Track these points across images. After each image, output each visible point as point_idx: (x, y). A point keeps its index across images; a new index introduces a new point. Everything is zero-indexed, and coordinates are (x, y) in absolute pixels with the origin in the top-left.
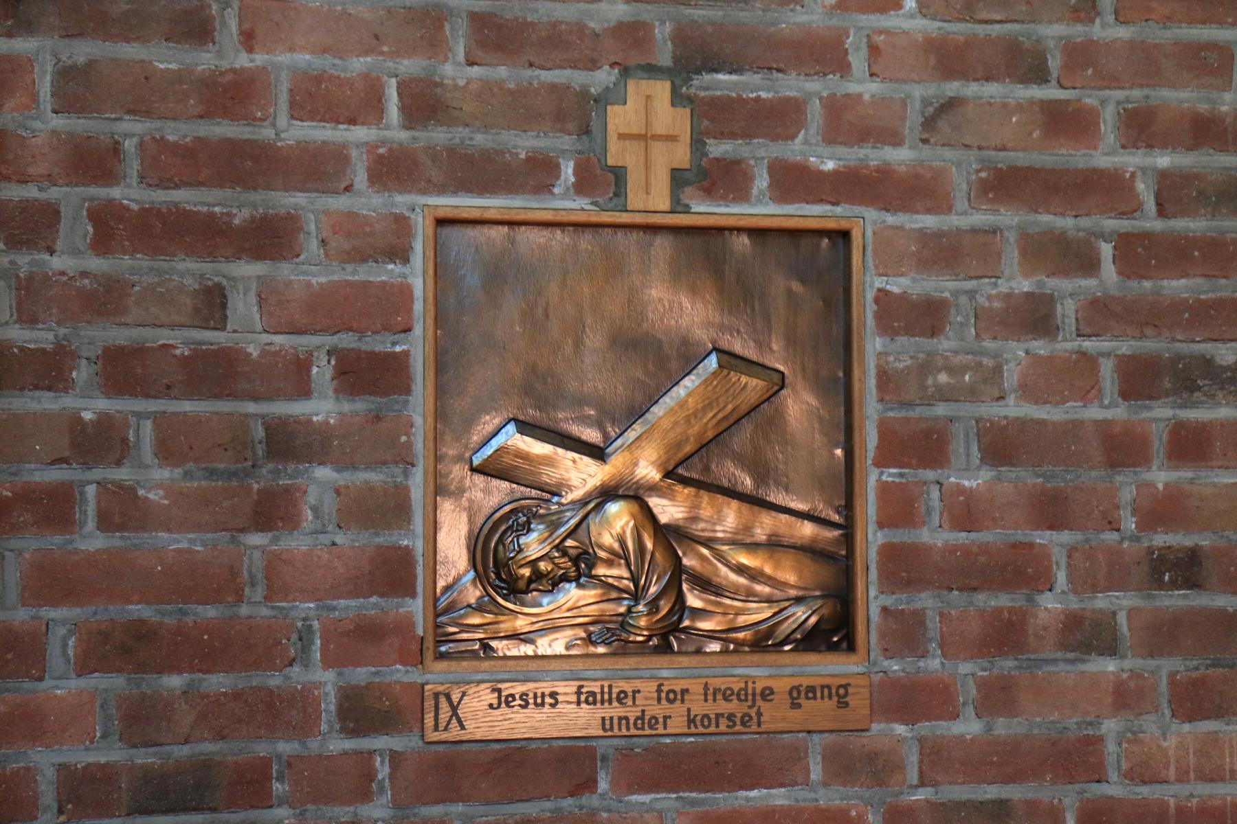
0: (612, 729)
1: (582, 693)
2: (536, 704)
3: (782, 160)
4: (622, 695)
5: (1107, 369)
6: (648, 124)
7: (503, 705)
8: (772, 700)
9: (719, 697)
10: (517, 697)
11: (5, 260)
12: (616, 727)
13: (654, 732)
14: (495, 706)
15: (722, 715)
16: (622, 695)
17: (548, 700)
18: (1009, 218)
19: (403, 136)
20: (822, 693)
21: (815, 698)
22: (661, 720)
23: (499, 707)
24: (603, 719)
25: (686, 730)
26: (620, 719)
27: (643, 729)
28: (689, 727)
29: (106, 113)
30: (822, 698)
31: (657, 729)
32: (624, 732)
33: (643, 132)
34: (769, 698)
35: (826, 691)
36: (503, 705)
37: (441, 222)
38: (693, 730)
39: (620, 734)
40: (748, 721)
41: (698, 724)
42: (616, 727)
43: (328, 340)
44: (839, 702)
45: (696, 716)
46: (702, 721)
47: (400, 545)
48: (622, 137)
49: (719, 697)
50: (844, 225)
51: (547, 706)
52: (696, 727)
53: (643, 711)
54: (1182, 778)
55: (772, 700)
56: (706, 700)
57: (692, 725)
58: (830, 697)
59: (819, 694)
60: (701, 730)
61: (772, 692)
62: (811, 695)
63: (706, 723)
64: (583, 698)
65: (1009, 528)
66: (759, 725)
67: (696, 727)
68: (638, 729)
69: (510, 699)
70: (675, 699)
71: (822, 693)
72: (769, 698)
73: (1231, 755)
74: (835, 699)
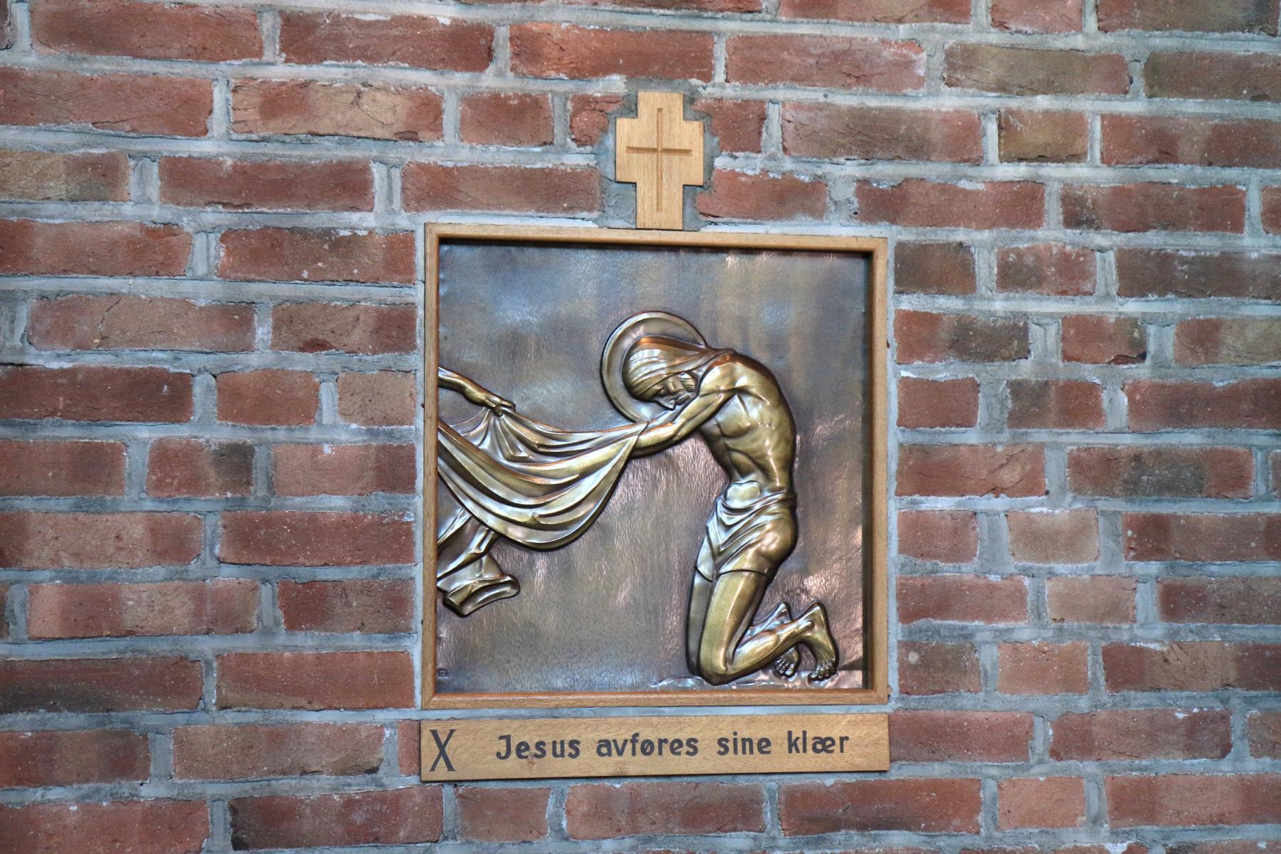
2: (555, 754)
4: (764, 744)
6: (659, 139)
7: (513, 755)
8: (769, 752)
9: (666, 748)
10: (684, 742)
11: (1171, 1)
16: (764, 744)
17: (568, 750)
20: (563, 750)
21: (609, 754)
23: (505, 757)
33: (655, 147)
34: (830, 749)
35: (558, 751)
36: (513, 755)
37: (444, 240)
48: (631, 149)
49: (666, 748)
50: (865, 245)
61: (768, 743)
65: (1189, 560)
69: (523, 748)
72: (830, 749)
73: (212, 815)
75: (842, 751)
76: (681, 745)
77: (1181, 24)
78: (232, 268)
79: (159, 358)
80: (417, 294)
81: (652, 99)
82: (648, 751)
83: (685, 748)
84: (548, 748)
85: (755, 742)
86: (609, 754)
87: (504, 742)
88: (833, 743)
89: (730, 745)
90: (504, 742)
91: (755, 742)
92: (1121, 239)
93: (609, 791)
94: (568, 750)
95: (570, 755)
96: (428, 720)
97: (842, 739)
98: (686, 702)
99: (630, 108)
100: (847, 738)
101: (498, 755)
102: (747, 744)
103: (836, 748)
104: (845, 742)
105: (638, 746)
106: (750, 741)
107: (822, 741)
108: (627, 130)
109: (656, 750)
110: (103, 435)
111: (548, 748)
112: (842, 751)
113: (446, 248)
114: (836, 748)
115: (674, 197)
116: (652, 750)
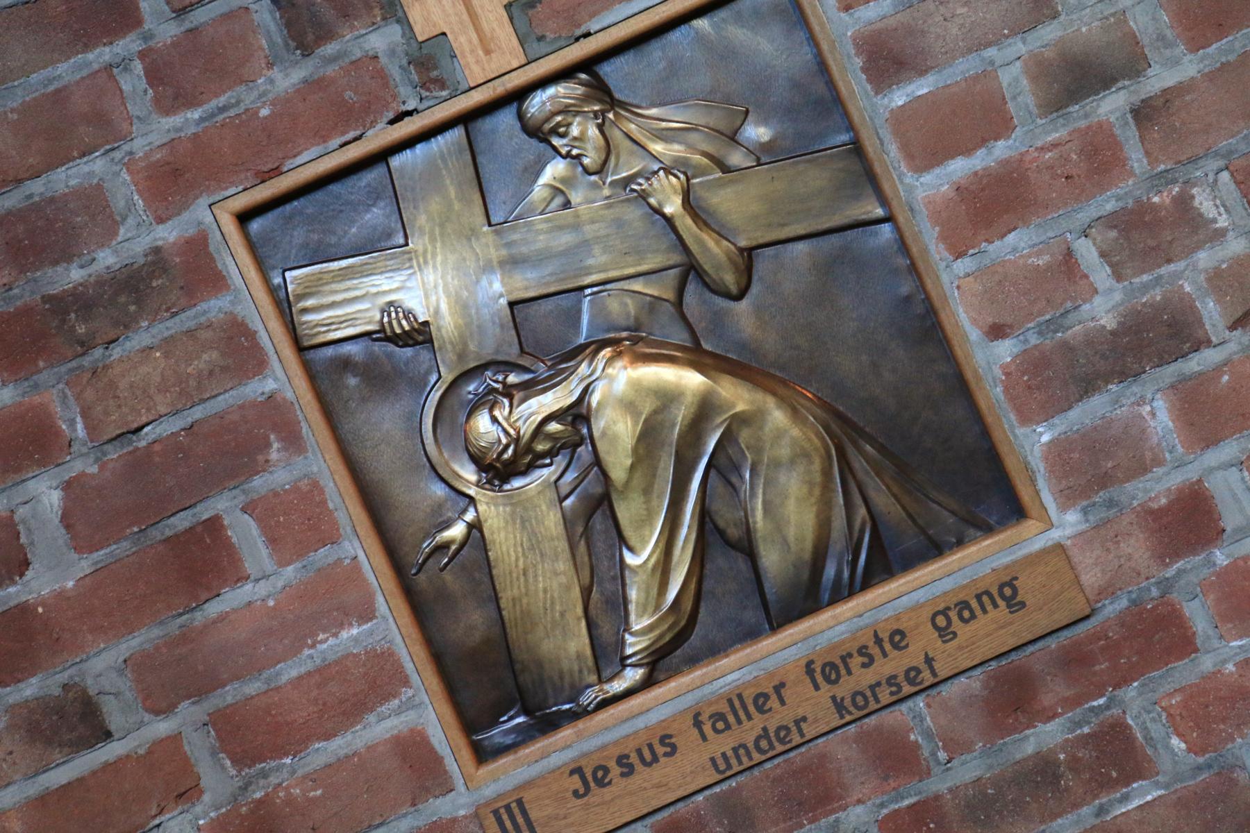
0: (729, 767)
4: (600, 774)
5: (1087, 252)
12: (734, 761)
13: (788, 746)
14: (582, 791)
15: (879, 684)
16: (897, 638)
17: (660, 750)
22: (869, 693)
23: (585, 795)
24: (713, 760)
26: (735, 750)
27: (772, 747)
28: (842, 717)
30: (739, 722)
32: (746, 763)
34: (606, 780)
38: (848, 718)
40: (785, 736)
41: (852, 709)
42: (734, 761)
44: (1009, 606)
45: (842, 699)
47: (1093, 340)
51: (663, 760)
52: (850, 713)
54: (956, 747)
55: (907, 646)
56: (704, 738)
58: (996, 606)
59: (731, 719)
62: (720, 725)
63: (859, 699)
64: (707, 728)
67: (850, 713)
68: (764, 752)
70: (839, 676)
74: (1001, 603)
75: (783, 703)
82: (833, 676)
83: (859, 660)
84: (634, 759)
85: (995, 592)
86: (973, 617)
87: (576, 777)
89: (875, 651)
90: (576, 777)
91: (995, 592)
92: (1018, 47)
94: (660, 750)
95: (666, 755)
96: (1212, 470)
98: (929, 578)
101: (576, 793)
102: (985, 598)
103: (774, 703)
104: (783, 691)
106: (987, 593)
109: (843, 672)
110: (204, 511)
111: (634, 759)
112: (783, 703)
113: (255, 226)
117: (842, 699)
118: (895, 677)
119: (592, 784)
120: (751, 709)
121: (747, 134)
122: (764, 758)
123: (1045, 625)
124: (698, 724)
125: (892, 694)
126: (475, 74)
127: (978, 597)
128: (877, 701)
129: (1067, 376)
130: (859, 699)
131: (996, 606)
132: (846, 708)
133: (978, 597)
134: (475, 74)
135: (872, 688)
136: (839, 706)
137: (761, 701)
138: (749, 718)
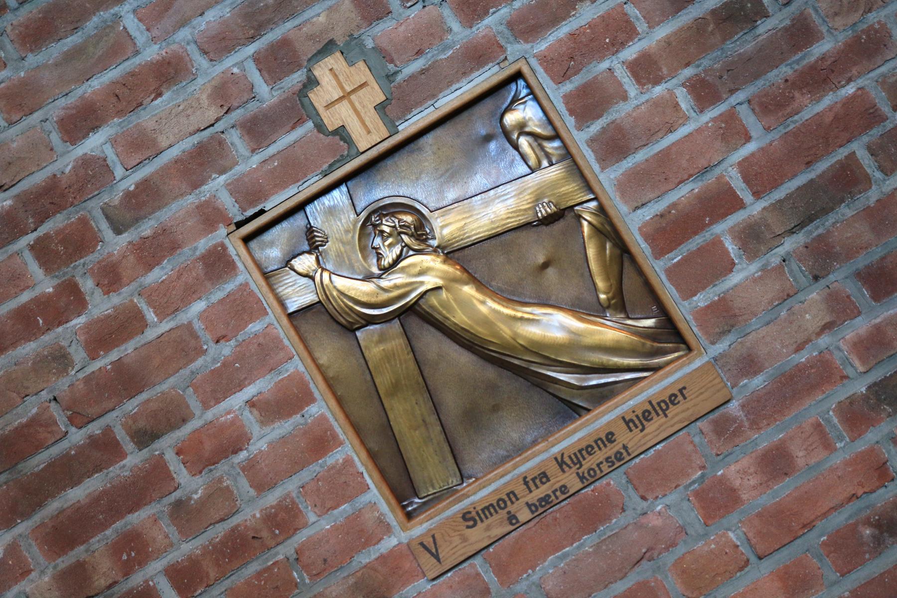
1: (528, 482)
3: (146, 64)
7: (671, 406)
13: (622, 462)
18: (151, 53)
19: (468, 32)
25: (581, 486)
28: (583, 483)
29: (499, 56)
31: (623, 459)
34: (676, 402)
36: (671, 406)
38: (586, 483)
39: (589, 482)
41: (588, 477)
43: (741, 96)
45: (583, 473)
46: (589, 474)
52: (587, 480)
53: (666, 416)
56: (631, 431)
57: (585, 481)
60: (592, 480)
61: (612, 434)
63: (592, 472)
66: (629, 454)
71: (510, 499)
72: (613, 439)
75: (685, 398)
76: (676, 396)
77: (219, 546)
78: (98, 384)
79: (55, 51)
80: (213, 350)
81: (321, 71)
88: (650, 413)
93: (659, 451)
97: (681, 391)
99: (312, 82)
100: (684, 388)
105: (531, 484)
107: (487, 508)
108: (319, 98)
109: (596, 449)
112: (685, 398)
114: (680, 398)
115: (373, 118)
116: (498, 505)
117: (583, 473)
118: (610, 457)
119: (606, 443)
120: (477, 518)
121: (509, 122)
122: (593, 480)
123: (619, 470)
124: (526, 483)
125: (609, 467)
126: (362, 146)
127: (596, 442)
128: (602, 471)
129: (270, 475)
130: (592, 472)
131: (658, 415)
132: (585, 478)
133: (596, 442)
134: (362, 146)
135: (598, 465)
136: (582, 478)
137: (673, 398)
138: (605, 446)
